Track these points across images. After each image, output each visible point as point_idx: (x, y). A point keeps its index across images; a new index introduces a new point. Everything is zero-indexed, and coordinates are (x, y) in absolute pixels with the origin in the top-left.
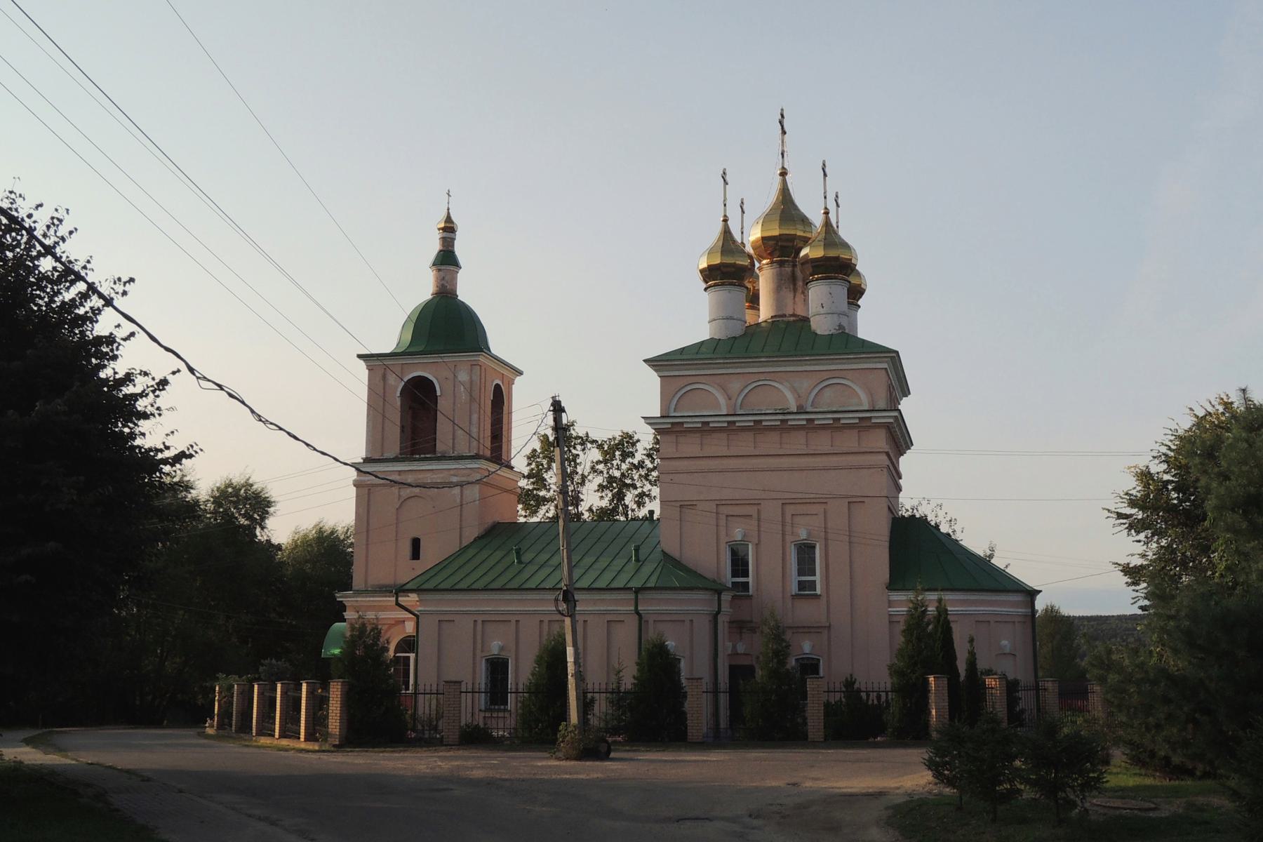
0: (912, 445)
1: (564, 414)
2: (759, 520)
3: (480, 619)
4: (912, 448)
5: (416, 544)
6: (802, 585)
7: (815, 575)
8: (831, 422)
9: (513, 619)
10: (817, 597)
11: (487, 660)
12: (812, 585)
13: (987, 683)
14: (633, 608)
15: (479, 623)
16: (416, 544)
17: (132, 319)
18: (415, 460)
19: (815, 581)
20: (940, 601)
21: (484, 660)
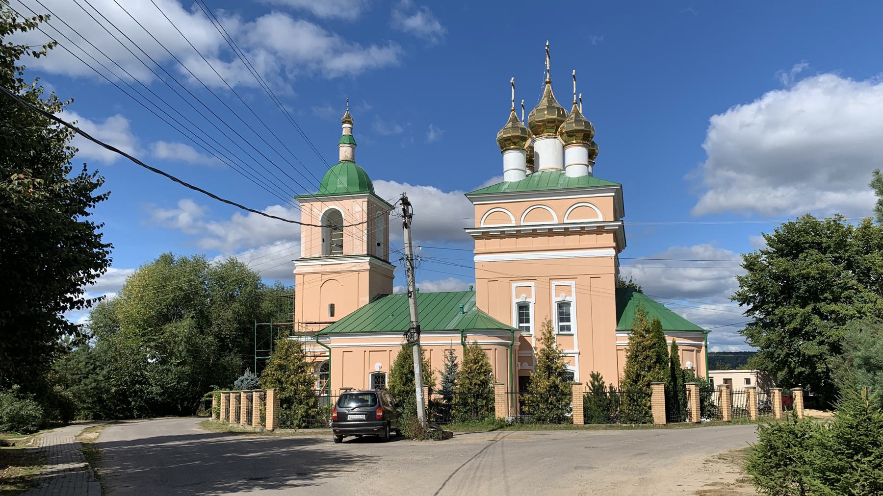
0: (626, 246)
1: (410, 207)
2: (57, 480)
3: (368, 349)
4: (626, 248)
5: (332, 307)
6: (562, 328)
7: (529, 323)
8: (580, 229)
9: (388, 349)
10: (572, 335)
11: (373, 375)
12: (568, 328)
13: (687, 387)
14: (460, 342)
15: (368, 352)
16: (332, 307)
17: (155, 172)
18: (330, 258)
19: (529, 326)
20: (674, 342)
21: (370, 374)
